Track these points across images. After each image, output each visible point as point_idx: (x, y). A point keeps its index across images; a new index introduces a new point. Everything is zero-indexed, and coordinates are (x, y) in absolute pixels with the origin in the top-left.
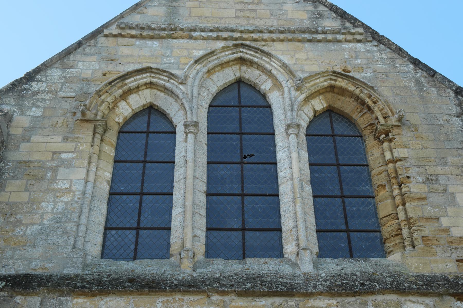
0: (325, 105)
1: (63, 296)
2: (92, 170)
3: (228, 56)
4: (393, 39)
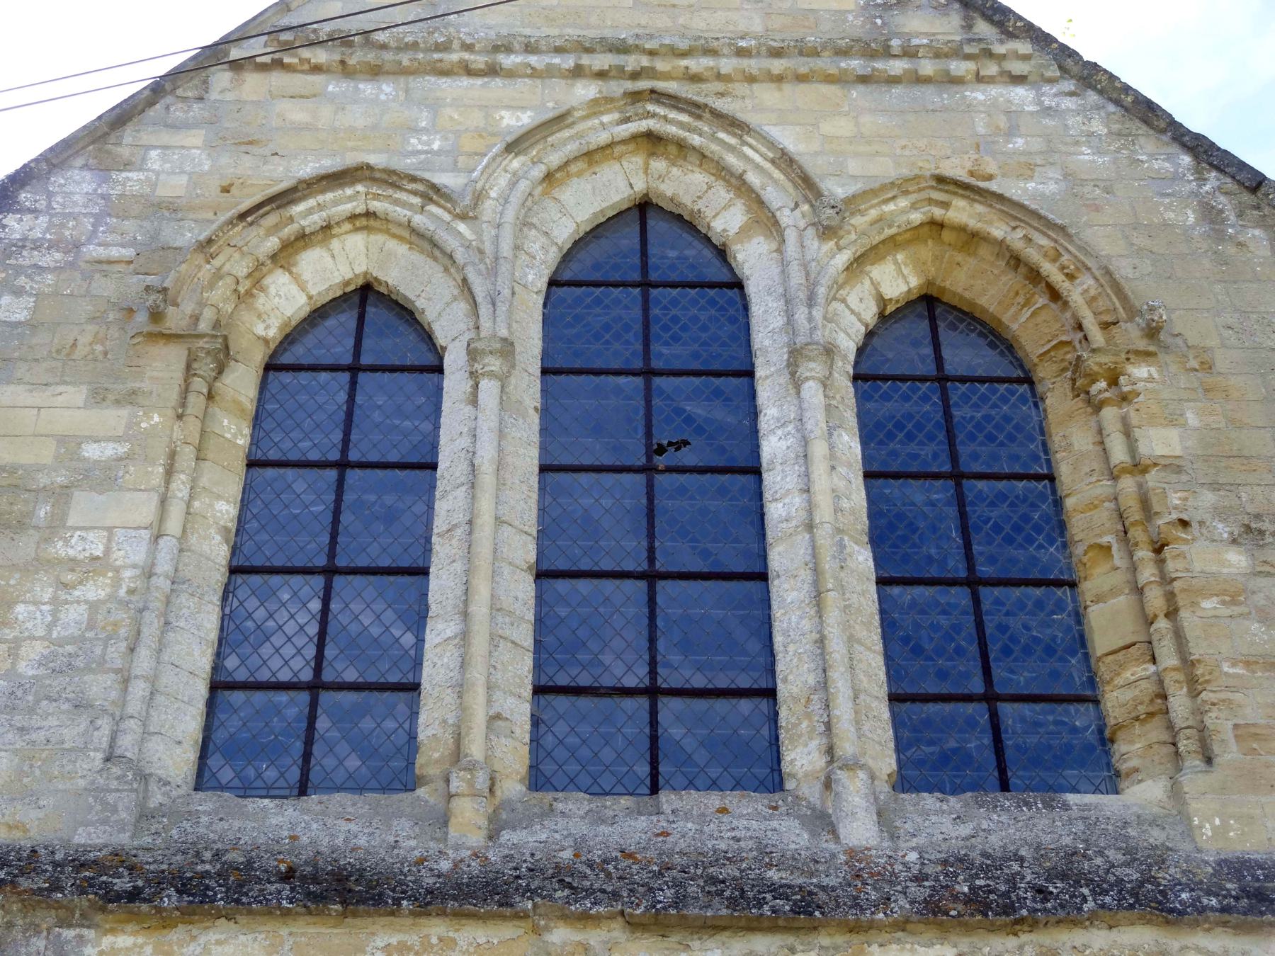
0: (914, 282)
1: (70, 926)
2: (175, 497)
3: (607, 127)
4: (1128, 76)
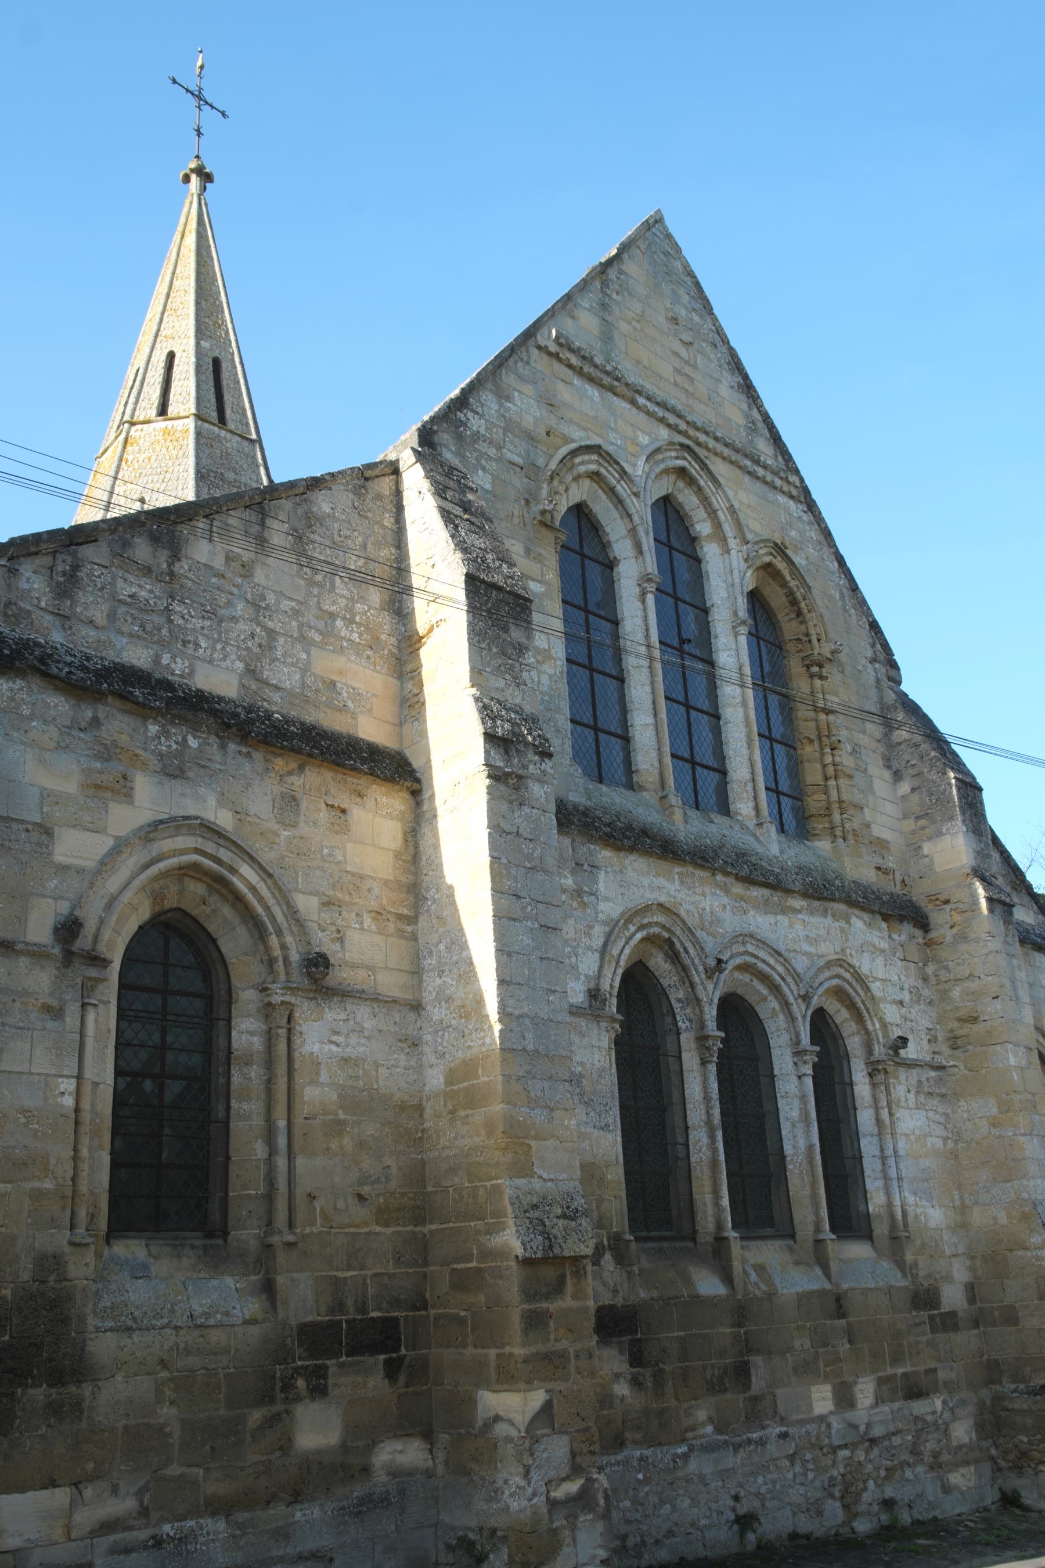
4: (825, 514)
